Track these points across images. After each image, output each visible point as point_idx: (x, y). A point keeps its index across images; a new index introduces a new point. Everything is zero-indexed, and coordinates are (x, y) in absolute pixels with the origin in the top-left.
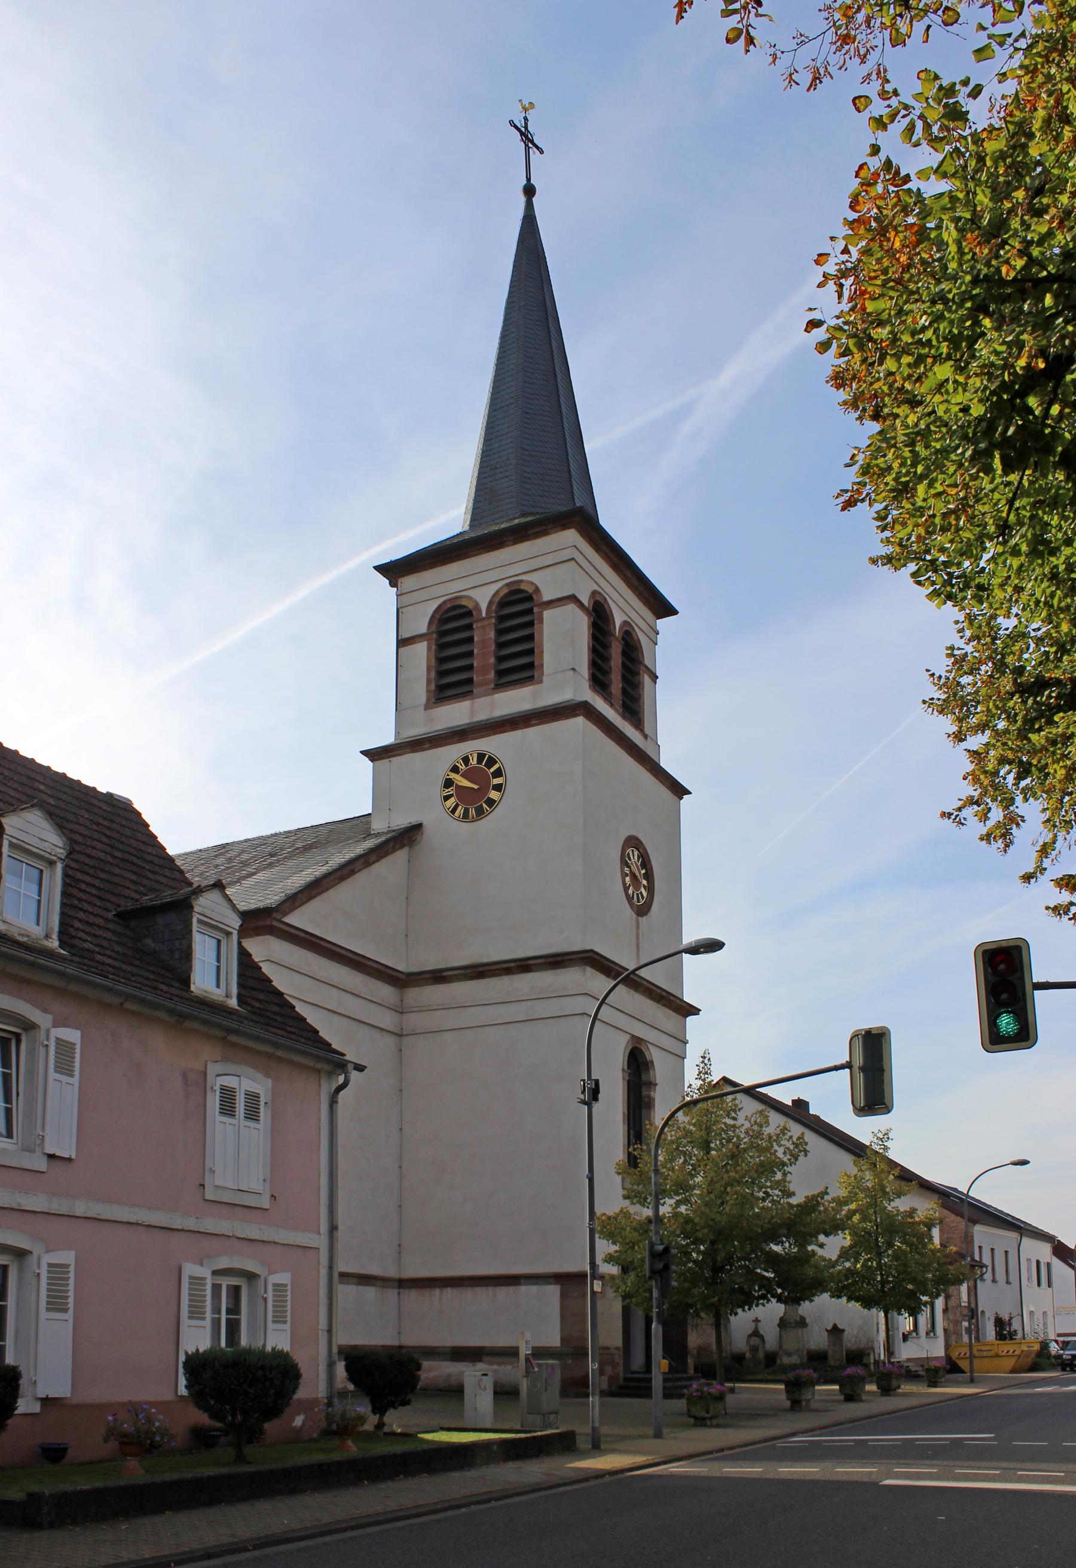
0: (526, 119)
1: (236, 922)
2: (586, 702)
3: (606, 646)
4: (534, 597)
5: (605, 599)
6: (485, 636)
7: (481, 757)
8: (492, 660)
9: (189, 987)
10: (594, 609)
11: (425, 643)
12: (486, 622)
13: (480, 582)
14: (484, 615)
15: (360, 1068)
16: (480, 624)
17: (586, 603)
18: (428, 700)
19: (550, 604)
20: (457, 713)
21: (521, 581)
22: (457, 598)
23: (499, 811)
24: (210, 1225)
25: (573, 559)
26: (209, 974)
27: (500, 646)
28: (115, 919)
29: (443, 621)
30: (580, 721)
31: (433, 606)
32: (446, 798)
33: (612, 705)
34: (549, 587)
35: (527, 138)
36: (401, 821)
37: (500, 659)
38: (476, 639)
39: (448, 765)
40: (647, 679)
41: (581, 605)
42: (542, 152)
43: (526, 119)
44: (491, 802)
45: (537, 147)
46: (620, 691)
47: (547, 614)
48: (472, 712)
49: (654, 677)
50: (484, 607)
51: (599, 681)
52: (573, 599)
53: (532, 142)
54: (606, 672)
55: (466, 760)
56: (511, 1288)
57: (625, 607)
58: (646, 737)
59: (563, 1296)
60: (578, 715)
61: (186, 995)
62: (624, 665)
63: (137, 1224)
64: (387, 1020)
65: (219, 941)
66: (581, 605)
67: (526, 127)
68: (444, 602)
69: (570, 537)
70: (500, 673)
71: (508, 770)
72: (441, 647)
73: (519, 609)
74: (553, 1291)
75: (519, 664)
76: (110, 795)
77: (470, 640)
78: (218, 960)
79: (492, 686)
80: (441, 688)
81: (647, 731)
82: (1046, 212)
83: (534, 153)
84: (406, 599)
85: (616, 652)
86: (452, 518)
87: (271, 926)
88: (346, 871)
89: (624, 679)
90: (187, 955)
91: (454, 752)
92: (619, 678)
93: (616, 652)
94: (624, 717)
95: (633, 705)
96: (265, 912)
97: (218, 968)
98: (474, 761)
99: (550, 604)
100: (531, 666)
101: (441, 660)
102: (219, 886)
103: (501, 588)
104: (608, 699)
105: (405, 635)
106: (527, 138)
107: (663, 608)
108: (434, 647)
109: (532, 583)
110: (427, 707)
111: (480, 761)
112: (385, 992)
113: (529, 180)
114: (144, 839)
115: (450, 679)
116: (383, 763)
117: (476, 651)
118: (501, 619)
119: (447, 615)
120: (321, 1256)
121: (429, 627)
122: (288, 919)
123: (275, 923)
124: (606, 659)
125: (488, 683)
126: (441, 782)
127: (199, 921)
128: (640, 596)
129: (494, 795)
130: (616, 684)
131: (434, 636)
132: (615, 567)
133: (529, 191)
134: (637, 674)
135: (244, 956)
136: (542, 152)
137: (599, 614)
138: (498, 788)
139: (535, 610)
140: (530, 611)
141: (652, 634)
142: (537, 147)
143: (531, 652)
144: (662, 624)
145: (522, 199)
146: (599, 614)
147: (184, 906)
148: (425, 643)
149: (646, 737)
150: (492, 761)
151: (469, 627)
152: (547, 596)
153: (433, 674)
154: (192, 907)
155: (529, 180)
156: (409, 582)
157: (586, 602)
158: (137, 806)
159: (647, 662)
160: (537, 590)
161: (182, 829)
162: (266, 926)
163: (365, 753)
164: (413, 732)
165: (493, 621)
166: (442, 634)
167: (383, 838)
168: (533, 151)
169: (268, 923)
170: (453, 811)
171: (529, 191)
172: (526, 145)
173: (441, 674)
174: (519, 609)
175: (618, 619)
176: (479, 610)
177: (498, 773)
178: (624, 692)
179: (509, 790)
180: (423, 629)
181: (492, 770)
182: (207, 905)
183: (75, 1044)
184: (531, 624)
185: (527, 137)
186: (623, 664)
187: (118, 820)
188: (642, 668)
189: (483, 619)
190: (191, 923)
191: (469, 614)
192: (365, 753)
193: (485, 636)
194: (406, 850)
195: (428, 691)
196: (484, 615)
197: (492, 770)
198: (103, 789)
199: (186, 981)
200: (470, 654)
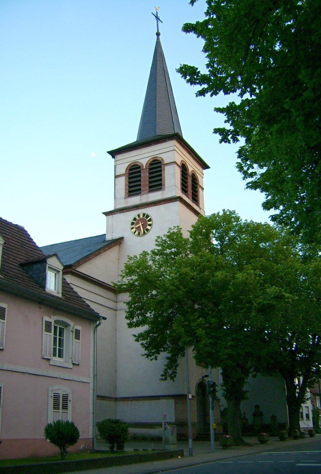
0: (157, 12)
1: (61, 268)
2: (180, 196)
3: (186, 179)
4: (162, 162)
5: (186, 163)
6: (145, 176)
7: (144, 215)
8: (148, 183)
9: (45, 289)
10: (182, 166)
11: (124, 177)
12: (145, 170)
13: (143, 157)
14: (144, 168)
15: (105, 319)
16: (143, 171)
17: (179, 164)
18: (126, 195)
19: (167, 164)
20: (135, 200)
21: (157, 157)
22: (135, 162)
23: (150, 233)
24: (51, 374)
25: (175, 150)
26: (52, 284)
27: (150, 178)
28: (19, 266)
29: (130, 170)
30: (178, 204)
31: (127, 165)
32: (132, 228)
33: (189, 198)
34: (166, 158)
35: (157, 18)
36: (116, 236)
37: (150, 182)
38: (142, 176)
39: (133, 218)
40: (200, 190)
41: (178, 165)
42: (162, 22)
43: (157, 12)
44: (148, 230)
45: (161, 21)
46: (191, 193)
47: (166, 168)
48: (141, 200)
49: (203, 189)
50: (144, 165)
51: (184, 189)
52: (175, 163)
53: (159, 19)
54: (186, 187)
55: (139, 216)
56: (157, 401)
57: (192, 166)
58: (200, 209)
59: (176, 403)
60: (177, 201)
61: (44, 292)
62: (192, 185)
63: (26, 373)
64: (111, 304)
65: (56, 274)
66: (178, 165)
67: (157, 15)
68: (131, 164)
69: (173, 144)
70: (150, 187)
71: (153, 219)
72: (130, 178)
73: (156, 166)
74: (172, 401)
75: (157, 184)
76: (17, 225)
77: (140, 176)
78: (55, 281)
79: (148, 191)
80: (130, 192)
81: (200, 207)
82: (305, 237)
83: (160, 23)
84: (118, 162)
85: (190, 181)
86: (132, 138)
87: (71, 271)
88: (97, 253)
89: (193, 189)
90: (44, 278)
91: (134, 214)
92: (191, 189)
93: (190, 181)
94: (193, 202)
95: (195, 198)
96: (70, 266)
97: (55, 283)
98: (141, 216)
99: (167, 164)
100: (161, 185)
101: (130, 183)
102: (55, 255)
103: (151, 159)
104: (187, 196)
105: (117, 174)
106: (157, 18)
107: (205, 166)
108: (127, 178)
109: (161, 158)
110: (125, 198)
111: (144, 216)
112: (111, 295)
113: (158, 31)
114: (28, 240)
115: (133, 189)
116: (110, 217)
117: (142, 180)
118: (150, 169)
119: (132, 168)
120: (91, 386)
121: (125, 172)
122: (77, 269)
123: (72, 270)
124: (186, 183)
125: (146, 190)
126: (130, 223)
127: (49, 267)
128: (198, 162)
129: (149, 227)
130: (190, 191)
131: (128, 175)
132: (189, 153)
133: (158, 34)
134: (197, 188)
135: (64, 279)
136: (162, 22)
137: (184, 168)
138: (150, 225)
139: (162, 166)
140: (160, 167)
141: (202, 175)
142: (161, 21)
143: (161, 180)
144: (205, 171)
145: (156, 37)
146: (184, 168)
147: (43, 261)
148: (124, 177)
149: (200, 209)
150: (148, 216)
151: (140, 172)
152: (166, 162)
153: (127, 187)
154: (46, 262)
155: (158, 31)
156: (119, 157)
157: (179, 164)
158: (26, 229)
159: (200, 184)
160: (163, 160)
161: (42, 237)
162: (70, 271)
163: (104, 213)
164: (119, 206)
165: (148, 170)
166: (130, 174)
167: (108, 243)
168: (159, 22)
169: (70, 270)
170: (135, 233)
171: (158, 34)
172: (157, 20)
173: (130, 187)
174: (156, 166)
175: (190, 169)
176: (143, 166)
177: (150, 220)
178: (193, 194)
179: (153, 226)
180: (124, 172)
181: (148, 219)
182: (53, 262)
183: (5, 309)
184: (161, 171)
185: (157, 18)
186: (192, 184)
187: (19, 233)
188: (198, 186)
189: (144, 169)
190: (46, 267)
191: (140, 167)
192: (104, 213)
193: (145, 176)
194: (118, 246)
195: (125, 193)
196: (144, 168)
197: (148, 219)
198: (14, 223)
199: (43, 287)
200: (140, 180)
